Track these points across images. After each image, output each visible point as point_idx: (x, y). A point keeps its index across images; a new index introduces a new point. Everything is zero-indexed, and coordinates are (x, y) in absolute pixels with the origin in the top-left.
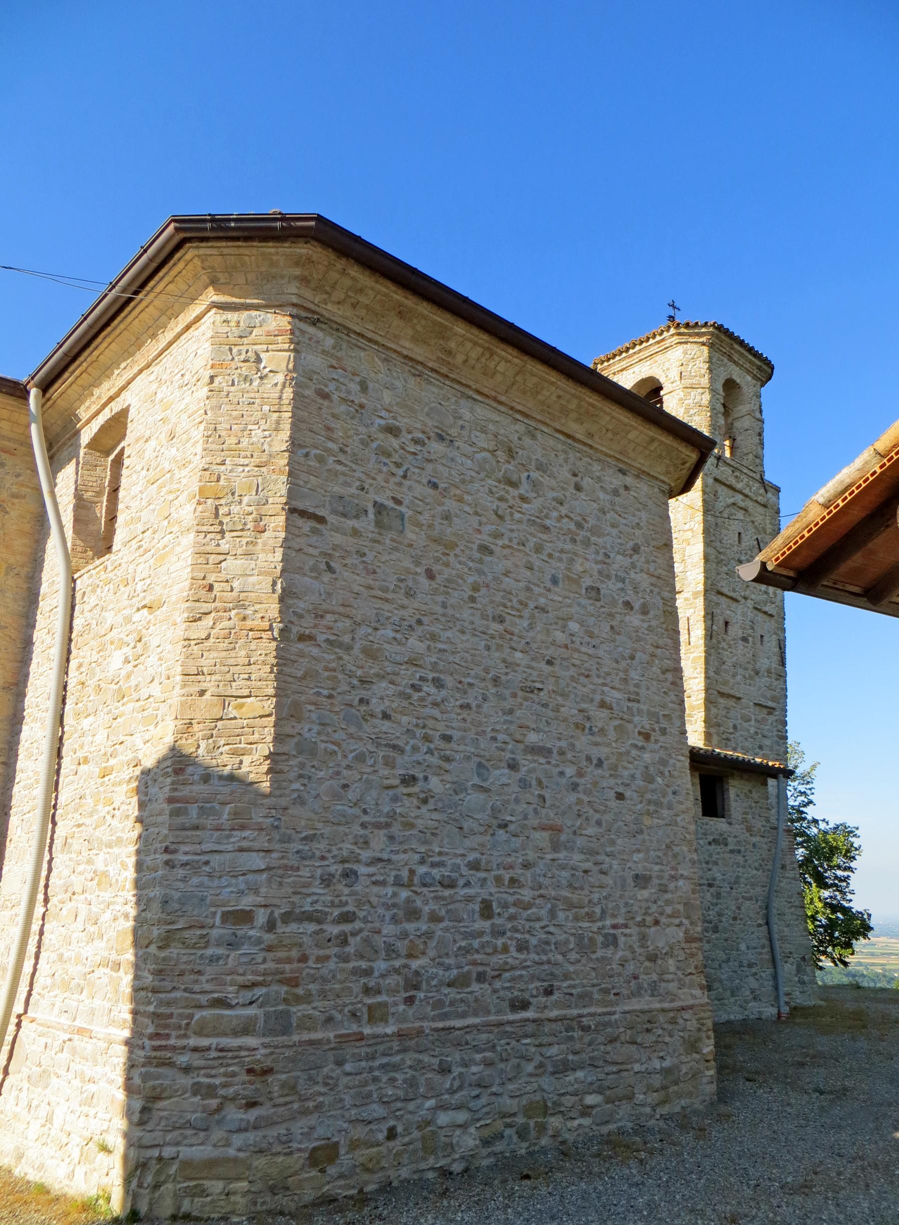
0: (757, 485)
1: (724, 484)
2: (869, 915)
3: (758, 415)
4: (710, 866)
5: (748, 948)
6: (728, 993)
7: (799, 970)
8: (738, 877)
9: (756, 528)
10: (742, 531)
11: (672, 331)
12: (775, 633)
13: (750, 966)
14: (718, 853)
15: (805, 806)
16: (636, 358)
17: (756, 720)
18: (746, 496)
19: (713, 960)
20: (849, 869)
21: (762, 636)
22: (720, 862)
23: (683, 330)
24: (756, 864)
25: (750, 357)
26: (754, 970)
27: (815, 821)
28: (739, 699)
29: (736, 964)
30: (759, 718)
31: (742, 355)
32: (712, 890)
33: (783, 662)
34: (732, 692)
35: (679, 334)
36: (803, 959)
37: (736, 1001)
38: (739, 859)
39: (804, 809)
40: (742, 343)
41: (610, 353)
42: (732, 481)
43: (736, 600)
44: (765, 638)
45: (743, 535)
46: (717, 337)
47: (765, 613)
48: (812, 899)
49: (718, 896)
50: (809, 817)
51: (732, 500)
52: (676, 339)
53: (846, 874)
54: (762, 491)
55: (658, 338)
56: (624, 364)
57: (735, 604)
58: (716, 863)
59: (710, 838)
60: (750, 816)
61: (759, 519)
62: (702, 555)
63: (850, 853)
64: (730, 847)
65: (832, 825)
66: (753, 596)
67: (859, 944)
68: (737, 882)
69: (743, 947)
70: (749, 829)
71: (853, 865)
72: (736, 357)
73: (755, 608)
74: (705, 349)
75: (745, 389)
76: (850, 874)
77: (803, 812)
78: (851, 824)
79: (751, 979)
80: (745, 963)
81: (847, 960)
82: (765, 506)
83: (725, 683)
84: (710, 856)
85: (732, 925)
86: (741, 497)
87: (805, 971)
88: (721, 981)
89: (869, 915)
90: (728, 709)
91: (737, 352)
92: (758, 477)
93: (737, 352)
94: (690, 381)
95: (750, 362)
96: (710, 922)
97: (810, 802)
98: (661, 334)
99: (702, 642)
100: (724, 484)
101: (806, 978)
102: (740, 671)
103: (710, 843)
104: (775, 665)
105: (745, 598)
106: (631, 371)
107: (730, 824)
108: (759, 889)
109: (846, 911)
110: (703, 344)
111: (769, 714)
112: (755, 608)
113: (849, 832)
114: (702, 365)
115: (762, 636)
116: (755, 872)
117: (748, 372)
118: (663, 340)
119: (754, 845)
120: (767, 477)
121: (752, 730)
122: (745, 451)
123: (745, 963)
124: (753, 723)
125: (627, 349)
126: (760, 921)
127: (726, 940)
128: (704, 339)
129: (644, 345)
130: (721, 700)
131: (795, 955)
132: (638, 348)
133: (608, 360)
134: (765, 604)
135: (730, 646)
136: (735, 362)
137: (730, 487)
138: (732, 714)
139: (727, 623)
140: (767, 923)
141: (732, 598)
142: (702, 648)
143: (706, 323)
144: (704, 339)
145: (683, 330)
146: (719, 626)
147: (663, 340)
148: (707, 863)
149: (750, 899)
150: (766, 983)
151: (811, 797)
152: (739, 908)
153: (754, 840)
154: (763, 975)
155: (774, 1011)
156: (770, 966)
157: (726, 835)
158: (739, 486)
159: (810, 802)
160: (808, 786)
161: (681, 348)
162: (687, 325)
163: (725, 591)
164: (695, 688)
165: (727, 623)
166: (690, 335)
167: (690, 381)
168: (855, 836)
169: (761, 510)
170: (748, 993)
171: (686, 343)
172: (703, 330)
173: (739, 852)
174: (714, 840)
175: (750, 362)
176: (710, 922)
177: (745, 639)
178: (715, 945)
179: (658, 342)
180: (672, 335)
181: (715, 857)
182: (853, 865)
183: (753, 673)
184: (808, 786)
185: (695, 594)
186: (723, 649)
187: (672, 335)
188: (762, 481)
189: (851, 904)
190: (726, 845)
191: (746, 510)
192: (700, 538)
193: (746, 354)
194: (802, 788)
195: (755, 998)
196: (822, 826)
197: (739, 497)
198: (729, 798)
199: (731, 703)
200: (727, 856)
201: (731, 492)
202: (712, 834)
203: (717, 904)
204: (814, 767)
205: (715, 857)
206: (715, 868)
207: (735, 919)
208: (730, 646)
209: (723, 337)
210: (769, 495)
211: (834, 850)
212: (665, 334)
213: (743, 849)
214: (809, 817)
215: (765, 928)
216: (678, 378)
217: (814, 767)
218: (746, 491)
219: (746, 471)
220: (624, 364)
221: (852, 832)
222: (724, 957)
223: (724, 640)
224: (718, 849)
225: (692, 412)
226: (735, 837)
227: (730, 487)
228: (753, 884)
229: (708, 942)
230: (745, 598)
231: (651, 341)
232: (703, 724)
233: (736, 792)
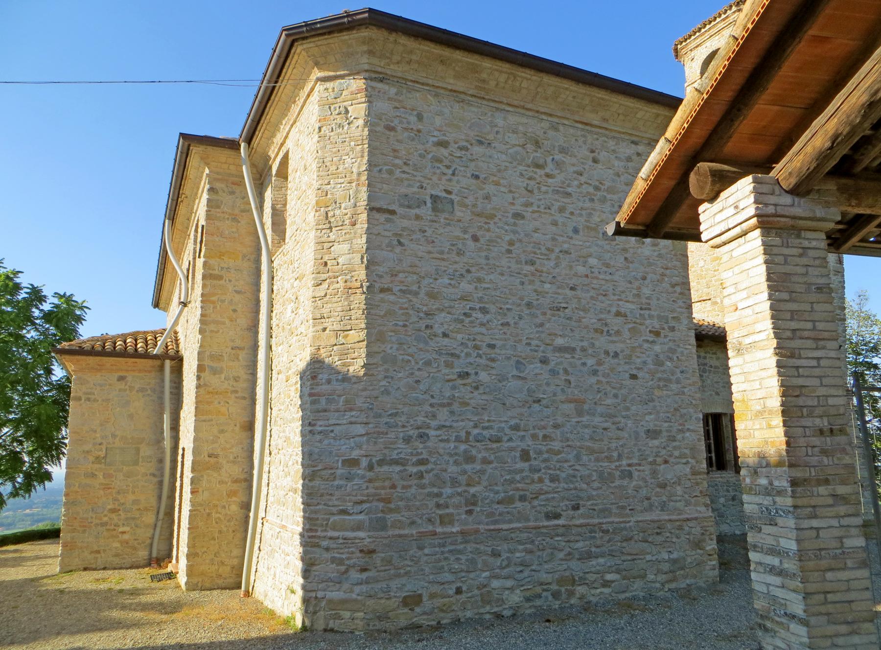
16: (707, 35)
55: (723, 16)
56: (698, 41)
106: (704, 46)
118: (727, 17)
125: (700, 29)
129: (713, 23)
133: (686, 40)
147: (727, 17)
179: (724, 20)
180: (734, 12)
187: (734, 12)
212: (729, 12)
220: (698, 41)
231: (718, 20)
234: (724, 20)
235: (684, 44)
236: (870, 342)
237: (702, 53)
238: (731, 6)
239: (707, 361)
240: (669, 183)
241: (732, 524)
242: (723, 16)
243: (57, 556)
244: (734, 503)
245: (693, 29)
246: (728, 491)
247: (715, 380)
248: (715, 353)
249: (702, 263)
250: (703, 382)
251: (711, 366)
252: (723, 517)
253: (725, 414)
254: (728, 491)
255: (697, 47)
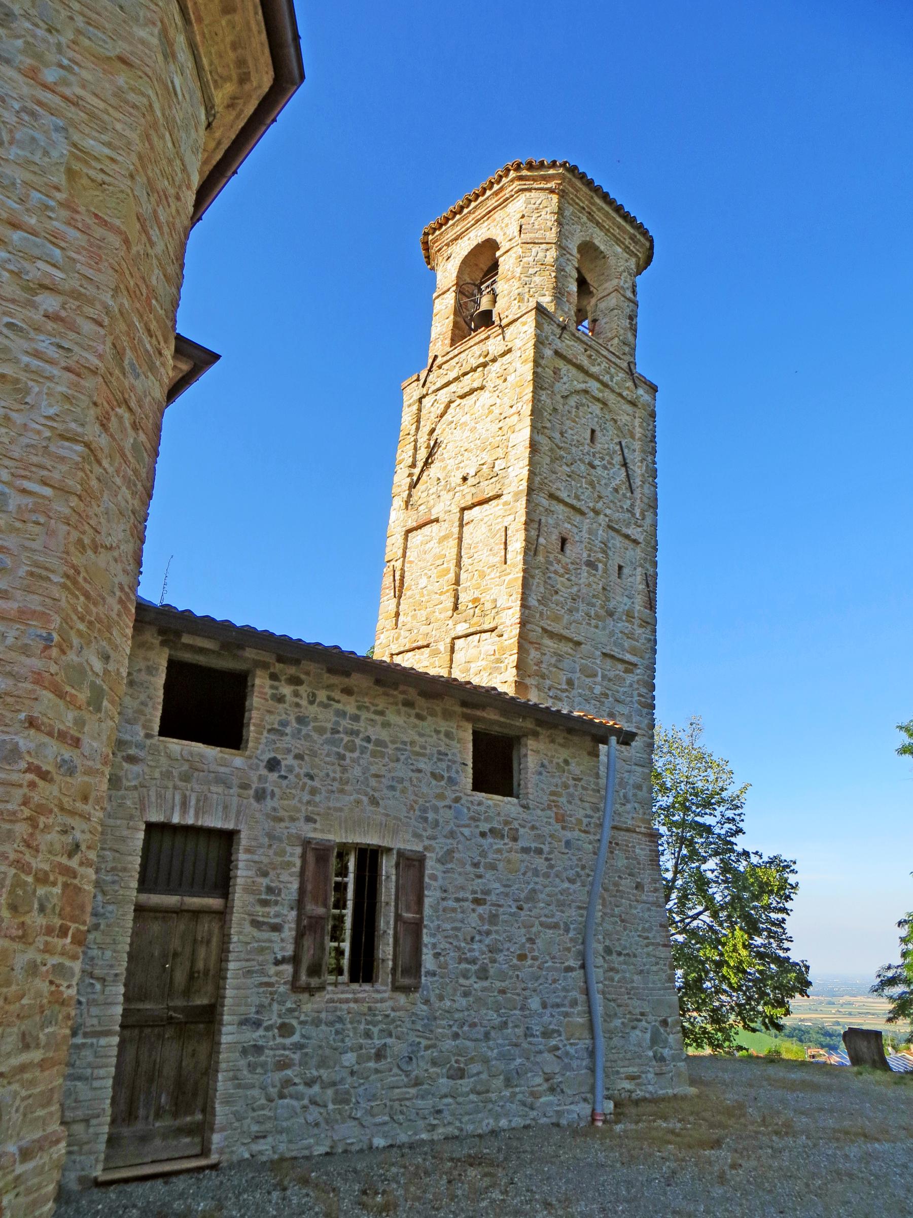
0: (622, 375)
1: (569, 362)
2: (807, 968)
3: (629, 294)
4: (481, 870)
5: (544, 1006)
6: (499, 1082)
7: (656, 1039)
8: (534, 891)
9: (619, 428)
10: (597, 428)
11: (512, 174)
12: (641, 566)
13: (546, 1034)
14: (499, 851)
15: (732, 835)
16: (471, 219)
17: (604, 677)
18: (605, 385)
19: (473, 1025)
20: (784, 910)
21: (620, 568)
22: (501, 866)
23: (525, 173)
24: (571, 873)
25: (619, 220)
26: (553, 1042)
27: (746, 854)
28: (578, 644)
29: (520, 1031)
30: (611, 674)
31: (607, 215)
32: (480, 909)
33: (651, 604)
34: (565, 633)
35: (520, 178)
36: (665, 1023)
37: (514, 1095)
38: (539, 862)
39: (733, 839)
40: (605, 197)
41: (440, 218)
42: (585, 363)
43: (582, 513)
44: (626, 571)
45: (598, 434)
46: (570, 182)
47: (627, 537)
48: (735, 945)
49: (493, 919)
50: (738, 848)
51: (583, 386)
52: (517, 185)
53: (780, 916)
54: (630, 384)
55: (496, 187)
56: (458, 229)
57: (578, 518)
58: (493, 867)
59: (485, 827)
60: (563, 800)
61: (624, 419)
62: (527, 443)
63: (785, 891)
64: (521, 843)
65: (765, 859)
66: (608, 512)
67: (796, 1002)
68: (532, 897)
69: (534, 1003)
70: (561, 819)
71: (788, 905)
72: (599, 216)
73: (609, 527)
74: (555, 198)
75: (612, 261)
76: (785, 916)
77: (732, 844)
78: (787, 856)
79: (547, 1056)
80: (537, 1029)
81: (782, 1022)
82: (633, 404)
83: (557, 619)
84: (483, 854)
85: (515, 968)
86: (597, 385)
87: (666, 1041)
88: (486, 1061)
89: (807, 968)
90: (560, 657)
91: (600, 209)
92: (624, 365)
93: (600, 209)
94: (532, 235)
95: (619, 227)
96: (473, 961)
97: (740, 831)
98: (499, 182)
99: (520, 557)
100: (569, 362)
101: (666, 1052)
102: (582, 607)
103: (483, 835)
104: (638, 605)
105: (597, 512)
106: (466, 238)
107: (526, 807)
108: (572, 912)
109: (783, 963)
110: (552, 191)
111: (626, 671)
112: (609, 527)
113: (785, 867)
114: (548, 217)
115: (620, 568)
116: (566, 885)
117: (618, 241)
118: (501, 189)
119: (568, 844)
120: (639, 369)
121: (598, 690)
122: (610, 335)
123: (537, 1029)
124: (599, 679)
125: (462, 208)
126: (571, 963)
127: (503, 992)
128: (552, 185)
129: (481, 199)
130: (547, 641)
131: (651, 1018)
132: (473, 204)
133: (441, 226)
134: (628, 525)
135: (568, 571)
136: (598, 224)
137: (580, 368)
138: (566, 664)
139: (564, 541)
140: (583, 966)
141: (572, 507)
142: (521, 566)
143: (554, 162)
144: (552, 185)
145: (525, 173)
146: (549, 541)
147: (501, 189)
148: (476, 865)
149: (555, 926)
150: (575, 1064)
151: (741, 825)
152: (531, 940)
153: (568, 835)
154: (572, 1051)
155: (586, 1109)
156: (586, 1034)
157: (515, 825)
158: (594, 369)
159: (740, 831)
160: (737, 812)
161: (523, 197)
162: (530, 166)
163: (563, 495)
164: (508, 623)
165: (564, 541)
166: (534, 179)
167: (532, 235)
168: (792, 871)
169: (628, 408)
170: (539, 1080)
171: (530, 190)
172: (551, 172)
173: (539, 852)
174: (492, 830)
175: (619, 227)
176: (473, 961)
177: (591, 564)
178: (478, 1000)
179: (496, 193)
180: (512, 181)
181: (491, 856)
182: (788, 905)
183: (602, 612)
184: (737, 812)
185: (517, 495)
186: (556, 572)
187: (512, 181)
188: (630, 372)
189: (789, 954)
190: (515, 839)
191: (605, 404)
192: (527, 421)
193: (614, 215)
194: (730, 814)
195: (552, 1090)
196: (754, 860)
197: (593, 386)
198: (526, 768)
199: (565, 648)
200: (514, 856)
201: (581, 376)
202: (488, 819)
203: (488, 933)
204: (744, 790)
205: (491, 856)
206: (489, 875)
207: (522, 957)
208: (568, 571)
209: (579, 184)
210: (640, 391)
211: (764, 888)
212: (504, 180)
213: (546, 848)
214: (738, 848)
215: (578, 974)
216: (517, 233)
217: (744, 790)
218: (606, 378)
219: (605, 353)
220: (458, 229)
221: (788, 866)
222: (498, 1021)
223: (559, 562)
224: (499, 844)
225: (532, 271)
226: (533, 828)
227: (580, 368)
228: (561, 904)
229: (466, 994)
230: (597, 512)
231: (488, 193)
232: (514, 671)
233: (534, 758)
234: (496, 193)
235: (437, 233)
236: (702, 791)
237: (463, 248)
238: (508, 170)
239: (361, 725)
240: (207, 195)
241: (368, 1120)
242: (496, 187)
243: (107, 1033)
244: (382, 1065)
245: (451, 208)
246: (368, 1035)
247: (374, 769)
248: (381, 713)
249: (423, 582)
250: (344, 770)
251: (368, 739)
252: (347, 1102)
253: (389, 850)
254: (368, 1035)
255: (456, 239)
